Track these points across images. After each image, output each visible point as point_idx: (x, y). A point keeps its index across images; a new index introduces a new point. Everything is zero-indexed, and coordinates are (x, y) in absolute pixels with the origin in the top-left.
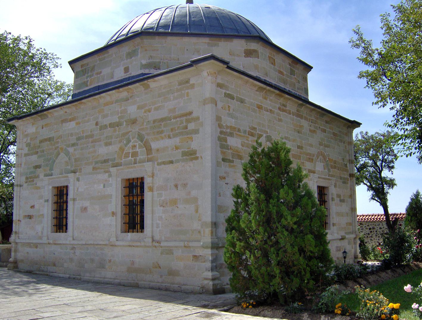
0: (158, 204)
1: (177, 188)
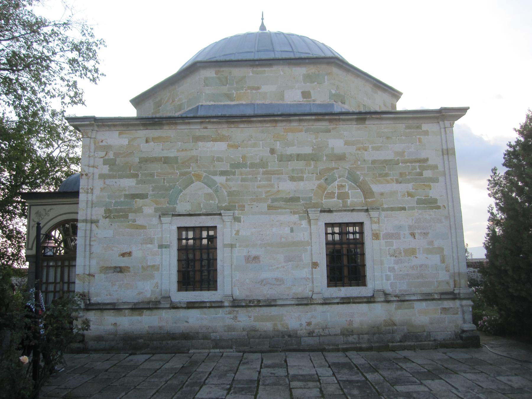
0: (388, 253)
1: (414, 236)
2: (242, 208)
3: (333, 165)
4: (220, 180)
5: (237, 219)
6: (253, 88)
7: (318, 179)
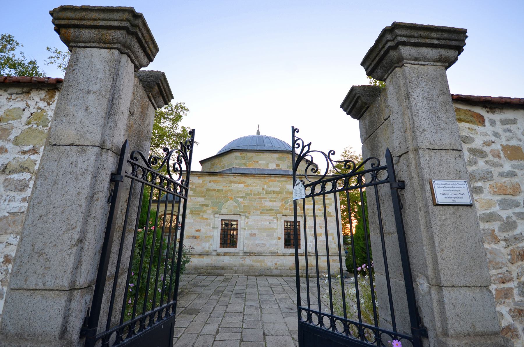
2: (249, 212)
3: (288, 196)
4: (241, 200)
5: (247, 217)
6: (255, 162)
7: (282, 202)
